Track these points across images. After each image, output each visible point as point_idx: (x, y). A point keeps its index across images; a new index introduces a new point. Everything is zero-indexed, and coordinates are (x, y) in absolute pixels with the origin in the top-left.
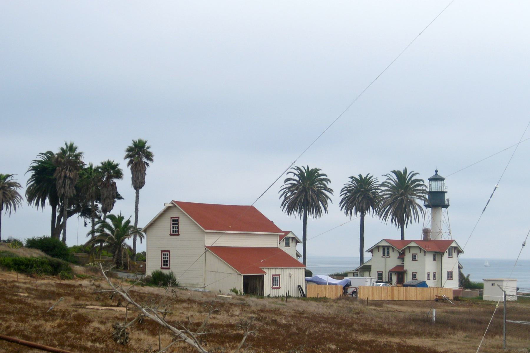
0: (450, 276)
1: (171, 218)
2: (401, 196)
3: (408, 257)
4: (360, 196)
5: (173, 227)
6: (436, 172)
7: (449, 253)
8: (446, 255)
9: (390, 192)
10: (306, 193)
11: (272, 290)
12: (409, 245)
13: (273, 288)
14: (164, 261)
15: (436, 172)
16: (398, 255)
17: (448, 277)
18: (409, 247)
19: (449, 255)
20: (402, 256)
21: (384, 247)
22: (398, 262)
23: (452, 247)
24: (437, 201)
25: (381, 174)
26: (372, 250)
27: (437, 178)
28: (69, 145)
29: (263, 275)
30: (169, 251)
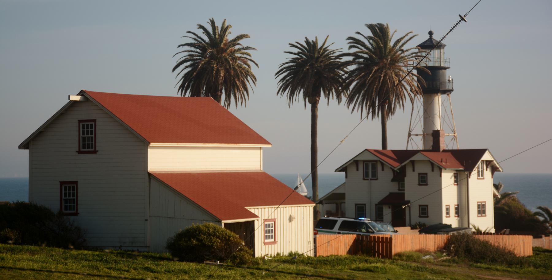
0: (482, 209)
1: (80, 121)
2: (374, 72)
3: (411, 179)
4: (310, 73)
5: (84, 139)
6: (431, 33)
7: (479, 172)
8: (474, 173)
9: (198, 50)
10: (214, 69)
11: (263, 246)
12: (412, 159)
13: (265, 244)
14: (66, 201)
15: (431, 33)
16: (391, 175)
17: (479, 212)
18: (413, 162)
19: (479, 175)
20: (399, 177)
21: (366, 162)
22: (394, 188)
23: (483, 161)
24: (432, 83)
25: (338, 38)
26: (346, 167)
27: (430, 45)
28: (226, 25)
29: (253, 221)
30: (76, 183)
